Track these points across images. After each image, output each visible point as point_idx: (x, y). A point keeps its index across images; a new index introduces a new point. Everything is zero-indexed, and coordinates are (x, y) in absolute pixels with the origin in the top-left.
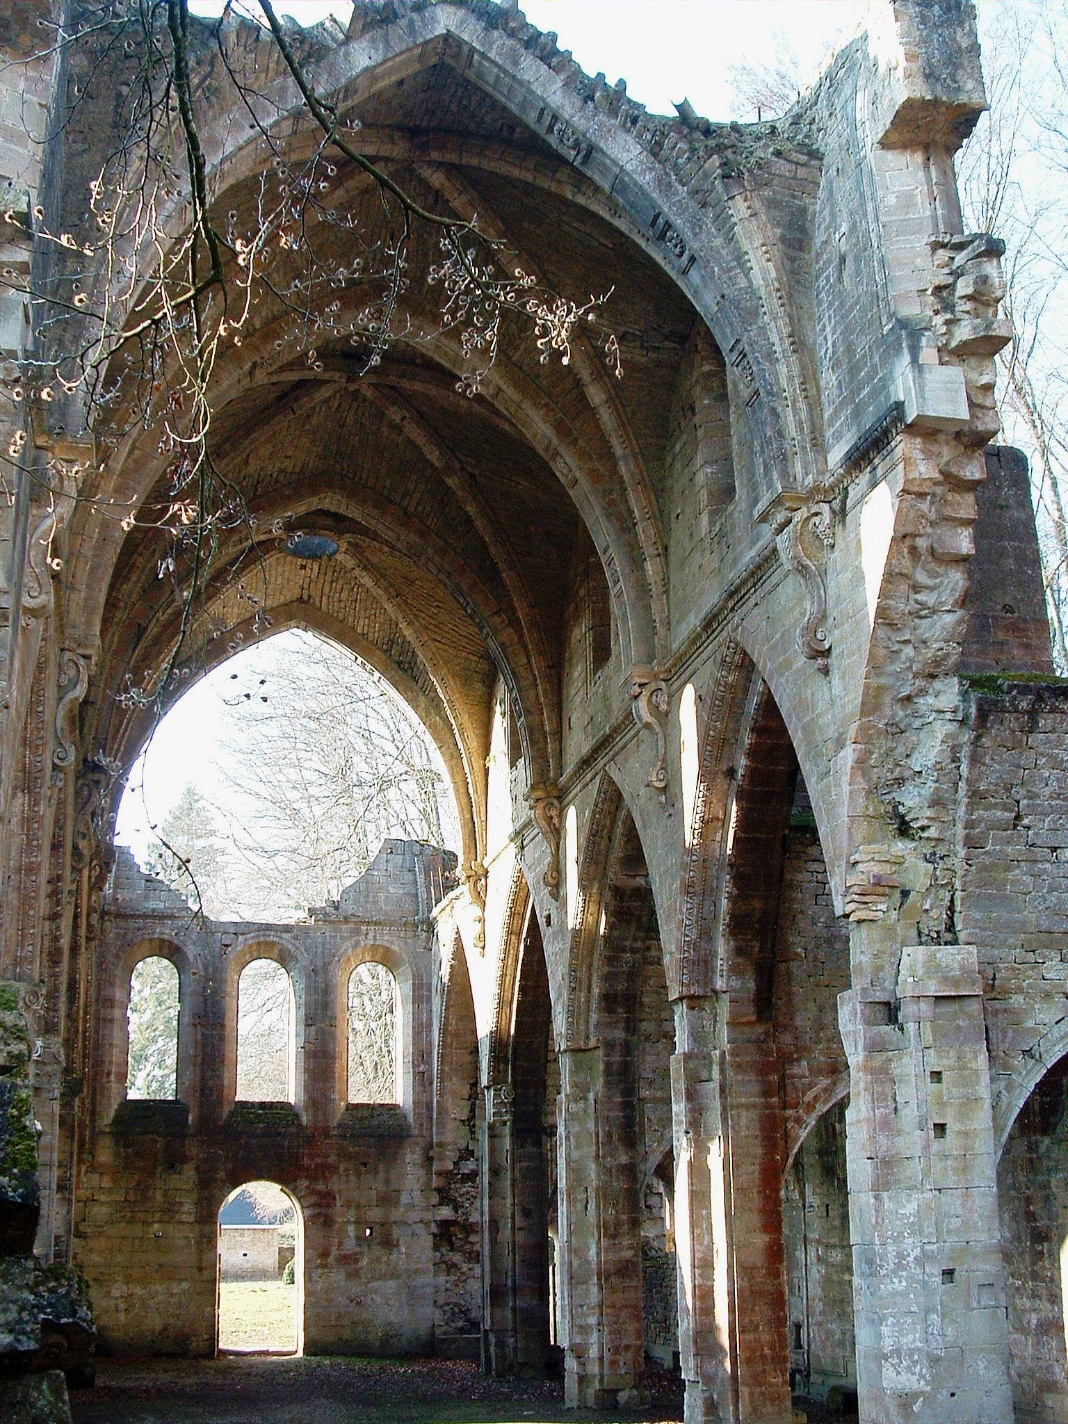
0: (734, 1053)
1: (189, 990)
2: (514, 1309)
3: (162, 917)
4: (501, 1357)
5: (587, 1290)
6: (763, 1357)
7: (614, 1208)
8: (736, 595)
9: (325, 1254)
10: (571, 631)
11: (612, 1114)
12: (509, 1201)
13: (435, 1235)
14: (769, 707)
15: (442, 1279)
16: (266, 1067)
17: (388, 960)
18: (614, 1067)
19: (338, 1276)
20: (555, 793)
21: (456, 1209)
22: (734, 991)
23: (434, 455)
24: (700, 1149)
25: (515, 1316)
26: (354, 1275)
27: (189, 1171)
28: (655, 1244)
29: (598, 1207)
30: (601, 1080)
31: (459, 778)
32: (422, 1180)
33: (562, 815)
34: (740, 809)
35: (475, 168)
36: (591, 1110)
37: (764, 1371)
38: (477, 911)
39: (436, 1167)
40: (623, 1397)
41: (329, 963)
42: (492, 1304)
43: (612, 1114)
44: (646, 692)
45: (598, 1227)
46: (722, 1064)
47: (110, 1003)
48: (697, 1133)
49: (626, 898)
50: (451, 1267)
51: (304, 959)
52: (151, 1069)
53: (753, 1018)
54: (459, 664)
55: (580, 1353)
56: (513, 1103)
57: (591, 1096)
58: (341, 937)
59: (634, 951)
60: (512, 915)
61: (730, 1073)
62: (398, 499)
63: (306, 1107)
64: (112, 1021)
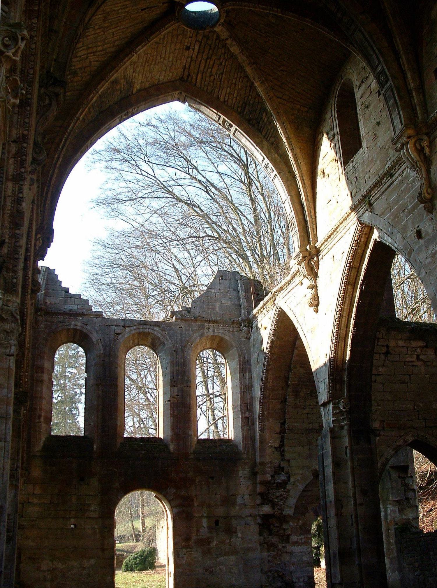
1: (93, 363)
2: (360, 565)
3: (74, 315)
9: (188, 539)
12: (350, 484)
13: (260, 525)
15: (265, 554)
16: (145, 416)
17: (221, 346)
19: (197, 554)
21: (273, 507)
26: (207, 553)
27: (95, 482)
31: (293, 193)
32: (250, 488)
38: (312, 282)
39: (259, 478)
41: (185, 346)
47: (41, 369)
50: (270, 546)
51: (169, 344)
52: (71, 414)
56: (349, 412)
58: (193, 330)
60: (351, 268)
63: (173, 440)
64: (42, 381)
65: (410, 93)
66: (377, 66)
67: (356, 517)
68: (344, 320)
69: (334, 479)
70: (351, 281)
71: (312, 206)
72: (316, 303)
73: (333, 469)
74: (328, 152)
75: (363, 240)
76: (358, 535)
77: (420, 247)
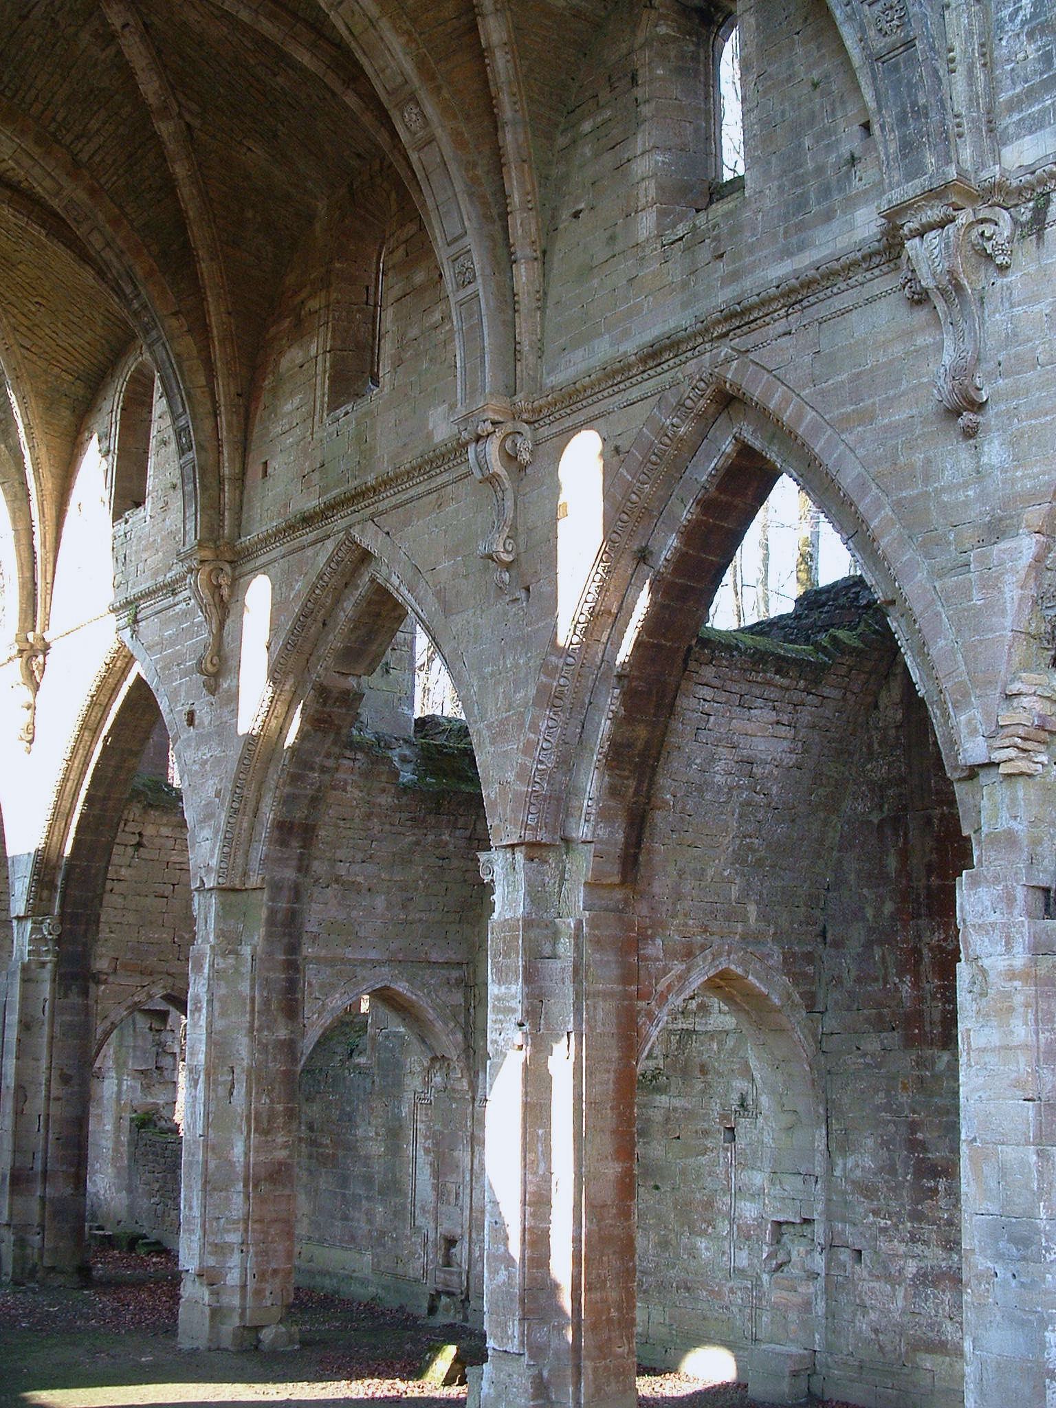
0: (593, 924)
2: (42, 1198)
4: (20, 1260)
5: (228, 1199)
6: (610, 1321)
7: (268, 1095)
10: (281, 353)
11: (272, 975)
12: (44, 1064)
18: (280, 916)
20: (228, 556)
22: (601, 842)
23: (150, 87)
24: (539, 1045)
25: (43, 1208)
28: (165, 1113)
29: (249, 1093)
30: (262, 931)
31: (21, 526)
33: (238, 585)
34: (653, 603)
36: (246, 969)
37: (610, 1339)
38: (26, 694)
40: (267, 1335)
42: (12, 1193)
43: (272, 975)
44: (499, 434)
45: (248, 1118)
46: (577, 936)
48: (536, 1026)
49: (330, 702)
53: (616, 879)
54: (46, 382)
55: (210, 1277)
57: (247, 951)
59: (324, 770)
60: (92, 705)
61: (587, 949)
62: (69, 138)
65: (221, 482)
66: (180, 416)
67: (47, 1121)
68: (69, 784)
69: (18, 1050)
70: (92, 724)
71: (52, 559)
72: (30, 737)
73: (19, 1032)
74: (95, 470)
75: (119, 664)
76: (46, 1150)
77: (189, 739)
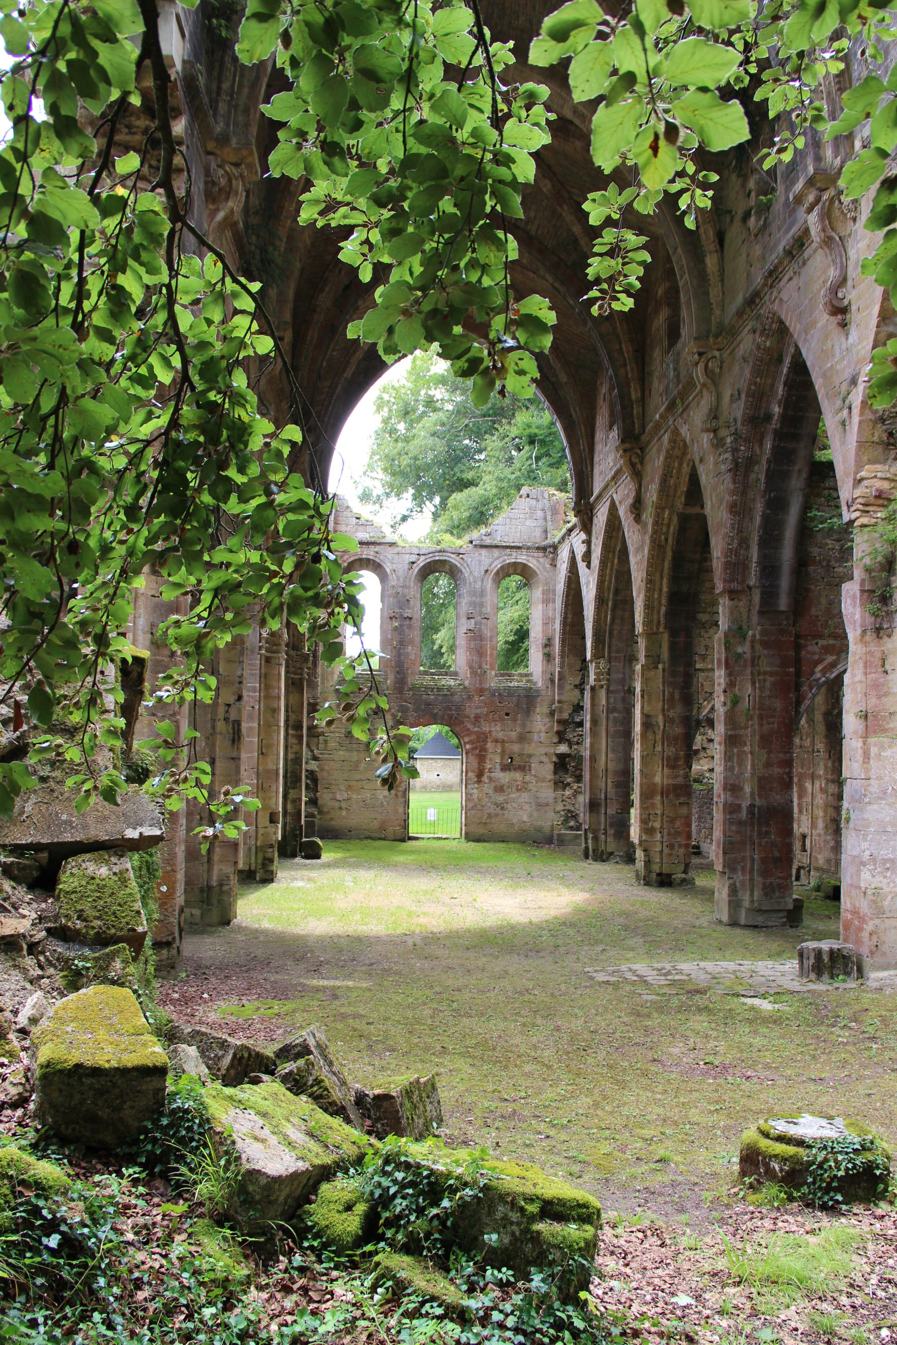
8: (774, 276)
14: (800, 368)
35: (786, 408)
